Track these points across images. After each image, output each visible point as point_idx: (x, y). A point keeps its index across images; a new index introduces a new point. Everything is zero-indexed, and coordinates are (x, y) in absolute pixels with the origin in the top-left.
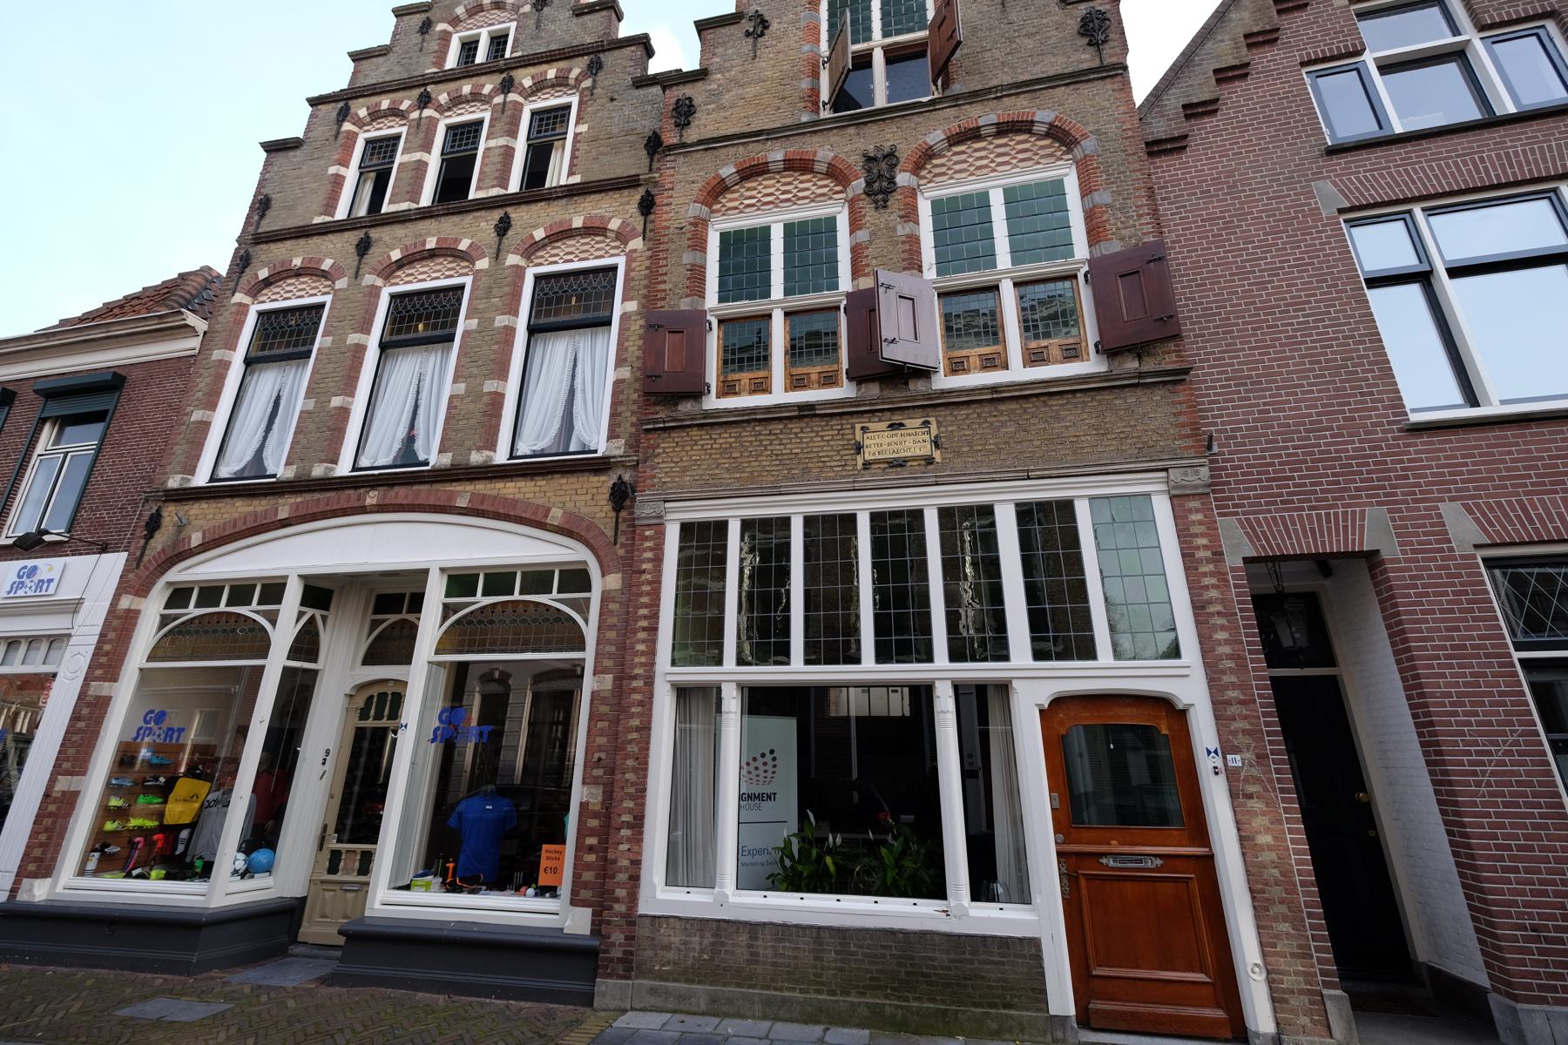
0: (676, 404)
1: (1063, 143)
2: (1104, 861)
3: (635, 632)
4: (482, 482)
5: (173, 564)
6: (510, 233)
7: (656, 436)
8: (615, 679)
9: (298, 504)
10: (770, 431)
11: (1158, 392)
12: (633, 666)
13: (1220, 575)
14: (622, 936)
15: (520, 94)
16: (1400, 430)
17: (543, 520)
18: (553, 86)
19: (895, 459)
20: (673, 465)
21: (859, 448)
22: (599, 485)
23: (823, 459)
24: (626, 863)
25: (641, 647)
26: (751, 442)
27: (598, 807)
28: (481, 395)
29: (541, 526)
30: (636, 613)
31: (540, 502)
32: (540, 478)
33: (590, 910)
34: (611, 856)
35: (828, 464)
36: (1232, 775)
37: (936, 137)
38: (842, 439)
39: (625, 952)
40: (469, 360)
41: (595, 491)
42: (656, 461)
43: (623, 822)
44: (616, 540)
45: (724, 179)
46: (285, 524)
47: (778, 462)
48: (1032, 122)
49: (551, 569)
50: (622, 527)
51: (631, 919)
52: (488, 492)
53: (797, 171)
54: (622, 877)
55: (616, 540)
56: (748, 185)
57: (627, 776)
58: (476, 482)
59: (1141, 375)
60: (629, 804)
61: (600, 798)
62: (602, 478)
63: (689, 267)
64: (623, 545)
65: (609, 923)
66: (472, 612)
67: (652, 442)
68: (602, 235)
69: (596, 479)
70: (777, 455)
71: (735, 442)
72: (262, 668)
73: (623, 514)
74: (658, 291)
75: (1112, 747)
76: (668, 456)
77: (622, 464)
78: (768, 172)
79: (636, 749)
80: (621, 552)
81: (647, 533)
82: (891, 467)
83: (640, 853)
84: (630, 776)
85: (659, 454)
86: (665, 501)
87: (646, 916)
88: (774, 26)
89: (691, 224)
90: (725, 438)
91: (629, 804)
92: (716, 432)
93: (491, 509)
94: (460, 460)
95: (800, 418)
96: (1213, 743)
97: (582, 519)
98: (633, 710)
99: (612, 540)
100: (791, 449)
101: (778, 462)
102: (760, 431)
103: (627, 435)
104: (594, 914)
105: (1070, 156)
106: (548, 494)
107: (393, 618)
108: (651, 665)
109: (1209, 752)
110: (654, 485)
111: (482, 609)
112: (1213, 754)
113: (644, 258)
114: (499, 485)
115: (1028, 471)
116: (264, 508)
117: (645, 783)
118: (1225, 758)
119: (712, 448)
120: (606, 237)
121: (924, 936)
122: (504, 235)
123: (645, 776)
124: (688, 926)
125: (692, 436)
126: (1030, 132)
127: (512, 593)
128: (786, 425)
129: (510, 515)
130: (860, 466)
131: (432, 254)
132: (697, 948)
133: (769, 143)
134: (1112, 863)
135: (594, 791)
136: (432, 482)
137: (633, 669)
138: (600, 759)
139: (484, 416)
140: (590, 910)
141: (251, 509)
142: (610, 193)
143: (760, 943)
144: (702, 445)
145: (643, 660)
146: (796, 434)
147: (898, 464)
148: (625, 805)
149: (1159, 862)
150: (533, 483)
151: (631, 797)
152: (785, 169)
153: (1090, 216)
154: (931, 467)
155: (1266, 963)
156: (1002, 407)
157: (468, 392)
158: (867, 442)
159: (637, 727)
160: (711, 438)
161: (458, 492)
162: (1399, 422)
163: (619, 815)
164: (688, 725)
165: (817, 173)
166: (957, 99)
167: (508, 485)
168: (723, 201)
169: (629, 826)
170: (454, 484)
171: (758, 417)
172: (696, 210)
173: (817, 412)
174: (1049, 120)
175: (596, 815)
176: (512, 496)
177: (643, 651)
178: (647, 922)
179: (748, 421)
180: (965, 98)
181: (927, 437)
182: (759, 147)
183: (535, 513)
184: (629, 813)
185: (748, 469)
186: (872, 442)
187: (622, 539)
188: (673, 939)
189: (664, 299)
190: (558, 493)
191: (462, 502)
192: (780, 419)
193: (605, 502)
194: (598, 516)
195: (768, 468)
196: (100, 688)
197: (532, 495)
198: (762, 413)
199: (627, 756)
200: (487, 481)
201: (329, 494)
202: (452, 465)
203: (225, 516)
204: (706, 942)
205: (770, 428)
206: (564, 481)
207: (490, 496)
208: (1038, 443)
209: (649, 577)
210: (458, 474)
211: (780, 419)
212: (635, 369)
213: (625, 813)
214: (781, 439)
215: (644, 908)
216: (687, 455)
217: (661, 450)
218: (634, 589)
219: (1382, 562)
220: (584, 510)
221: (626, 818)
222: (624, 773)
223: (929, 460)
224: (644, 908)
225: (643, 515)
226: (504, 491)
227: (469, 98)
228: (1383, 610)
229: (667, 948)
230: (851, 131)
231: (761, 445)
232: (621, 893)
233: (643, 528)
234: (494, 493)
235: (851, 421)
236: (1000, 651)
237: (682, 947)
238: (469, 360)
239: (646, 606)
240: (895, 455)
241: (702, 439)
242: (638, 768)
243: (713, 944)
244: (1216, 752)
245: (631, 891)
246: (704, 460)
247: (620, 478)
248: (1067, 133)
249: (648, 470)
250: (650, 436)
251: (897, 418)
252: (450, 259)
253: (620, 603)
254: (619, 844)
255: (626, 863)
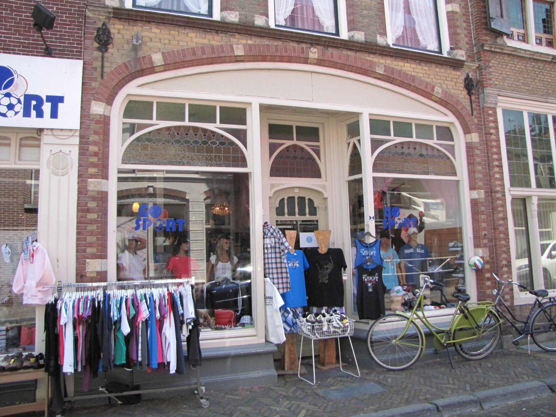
5: (133, 79)
9: (250, 46)
12: (496, 186)
22: (457, 77)
29: (428, 95)
43: (503, 264)
46: (237, 59)
47: (542, 85)
52: (395, 67)
60: (504, 256)
61: (488, 254)
64: (476, 117)
66: (150, 133)
69: (454, 73)
75: (524, 409)
79: (503, 229)
80: (476, 121)
84: (503, 242)
86: (499, 95)
92: (516, 60)
99: (471, 113)
100: (547, 79)
101: (542, 85)
107: (288, 143)
111: (396, 146)
116: (219, 44)
135: (485, 250)
138: (485, 235)
141: (206, 41)
144: (511, 67)
145: (94, 227)
160: (514, 64)
163: (501, 261)
164: (542, 210)
167: (406, 64)
170: (371, 56)
176: (410, 73)
177: (498, 178)
184: (505, 260)
191: (380, 71)
196: (93, 184)
197: (422, 75)
199: (500, 233)
201: (276, 43)
203: (182, 43)
214: (543, 73)
215: (516, 303)
221: (504, 262)
224: (516, 303)
226: (404, 68)
233: (488, 109)
234: (399, 68)
241: (510, 63)
249: (487, 75)
250: (486, 54)
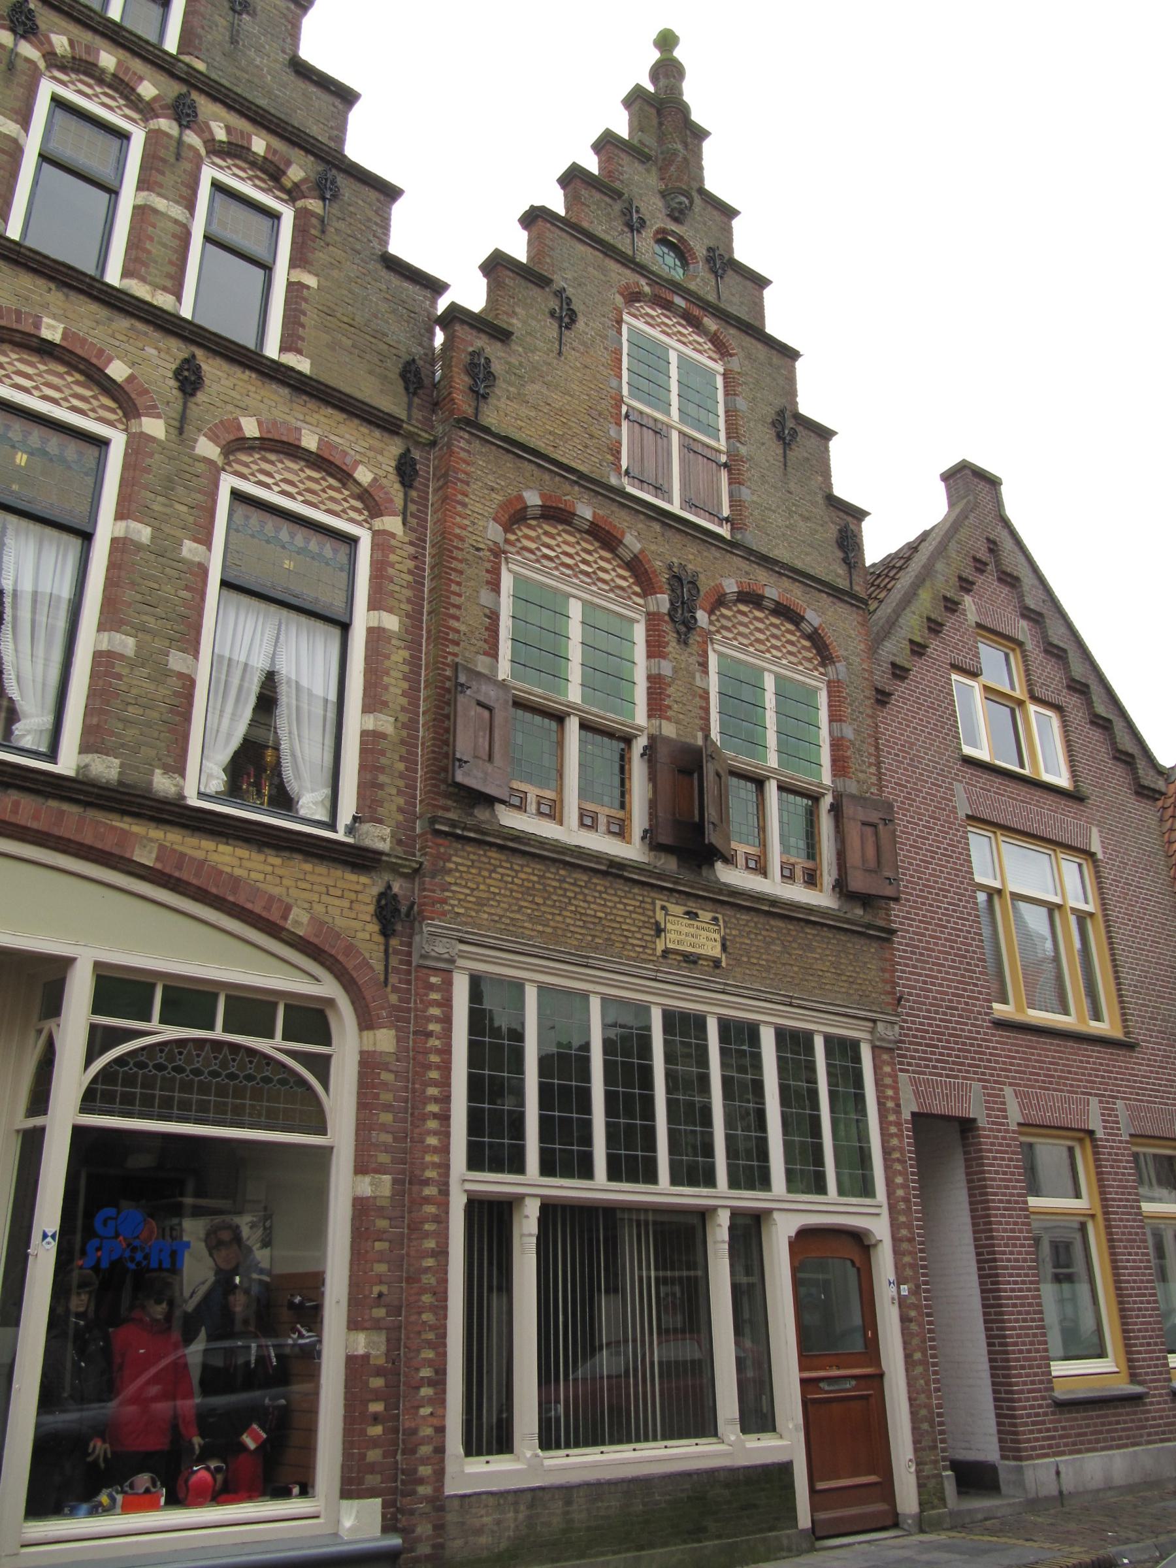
0: (473, 806)
1: (819, 653)
2: (822, 1385)
3: (424, 1118)
4: (177, 830)
6: (200, 397)
7: (446, 842)
8: (395, 1182)
10: (575, 879)
11: (874, 945)
12: (424, 1167)
13: (898, 1124)
14: (430, 1527)
15: (205, 143)
16: (990, 1022)
17: (280, 922)
18: (253, 164)
19: (692, 954)
20: (468, 891)
21: (659, 931)
22: (359, 888)
23: (626, 933)
24: (429, 1431)
25: (432, 1141)
26: (555, 888)
27: (381, 1361)
28: (167, 673)
29: (273, 930)
30: (424, 1092)
31: (276, 891)
32: (273, 852)
33: (379, 1501)
34: (406, 1422)
35: (630, 941)
36: (902, 1302)
37: (731, 586)
38: (643, 914)
39: (434, 1546)
40: (139, 597)
41: (353, 896)
42: (448, 879)
44: (386, 979)
45: (621, 542)
47: (581, 923)
48: (803, 618)
49: (272, 999)
50: (394, 962)
51: (438, 1502)
52: (189, 852)
53: (598, 541)
54: (425, 1450)
55: (386, 979)
56: (547, 528)
57: (424, 1317)
58: (168, 828)
59: (869, 926)
60: (429, 1354)
61: (383, 1348)
62: (364, 879)
63: (487, 611)
64: (395, 990)
65: (412, 1512)
67: (442, 850)
68: (340, 480)
69: (353, 877)
70: (581, 914)
71: (539, 883)
72: (42, 1130)
73: (394, 942)
74: (449, 628)
76: (461, 877)
77: (394, 869)
78: (570, 524)
79: (433, 1281)
80: (393, 998)
81: (433, 980)
82: (686, 961)
83: (443, 1417)
85: (451, 870)
87: (456, 1496)
88: (580, 324)
89: (490, 550)
90: (529, 873)
91: (429, 1354)
92: (518, 861)
93: (195, 882)
94: (133, 777)
95: (605, 874)
96: (892, 1277)
97: (338, 935)
98: (427, 1227)
99: (382, 978)
100: (596, 911)
102: (565, 877)
103: (393, 823)
104: (385, 1505)
105: (640, 601)
106: (285, 882)
108: (445, 1167)
109: (45, 1236)
110: (444, 914)
112: (49, 1239)
113: (405, 554)
114: (208, 844)
115: (791, 997)
117: (445, 1327)
118: (899, 1288)
119: (512, 883)
120: (344, 485)
121: (711, 1475)
122: (193, 395)
123: (445, 1317)
124: (502, 1501)
125: (490, 858)
126: (797, 624)
127: (211, 1027)
128: (590, 879)
129: (224, 900)
130: (659, 953)
131: (45, 350)
132: (512, 1525)
133: (576, 488)
134: (827, 1388)
136: (87, 804)
137: (423, 1170)
138: (380, 1295)
139: (171, 712)
140: (379, 1501)
142: (357, 421)
143: (575, 1507)
144: (503, 875)
146: (600, 892)
147: (691, 959)
148: (423, 1355)
149: (853, 1383)
150: (261, 857)
151: (430, 1345)
152: (587, 532)
153: (837, 745)
154: (717, 971)
155: (917, 1457)
156: (773, 922)
157: (142, 659)
158: (669, 926)
159: (433, 1250)
160: (511, 869)
161: (136, 835)
162: (987, 1014)
163: (417, 1370)
165: (617, 556)
166: (751, 554)
167: (222, 848)
168: (520, 534)
169: (431, 1383)
170: (127, 819)
171: (568, 859)
172: (495, 532)
173: (626, 874)
174: (816, 625)
175: (379, 1372)
177: (435, 1147)
178: (456, 1503)
179: (554, 860)
180: (756, 557)
181: (717, 936)
182: (567, 487)
183: (267, 908)
185: (552, 923)
186: (673, 927)
187: (393, 979)
188: (486, 1520)
189: (457, 644)
190: (300, 884)
191: (146, 857)
192: (586, 869)
193: (368, 918)
194: (360, 935)
195: (572, 928)
197: (261, 877)
198: (571, 856)
200: (153, 825)
202: (120, 783)
204: (521, 1516)
205: (575, 876)
206: (308, 867)
207: (192, 859)
208: (796, 969)
209: (437, 1043)
210: (140, 805)
211: (586, 869)
212: (399, 725)
213: (424, 1366)
214: (585, 895)
215: (451, 1489)
216: (484, 883)
217: (452, 866)
218: (420, 1057)
219: (978, 1129)
220: (340, 923)
222: (420, 1313)
223: (716, 963)
224: (451, 1489)
225: (433, 954)
227: (108, 79)
228: (967, 1167)
229: (479, 1532)
230: (657, 527)
231: (564, 896)
232: (425, 1471)
234: (199, 855)
235: (652, 895)
236: (763, 1181)
237: (495, 1528)
238: (139, 597)
239: (435, 1083)
240: (693, 950)
242: (437, 1307)
243: (529, 1517)
244: (53, 1237)
245: (436, 1467)
246: (505, 896)
247: (389, 887)
248: (826, 647)
251: (692, 905)
252: (78, 377)
253: (396, 1073)
254: (418, 1407)
255: (429, 1431)
